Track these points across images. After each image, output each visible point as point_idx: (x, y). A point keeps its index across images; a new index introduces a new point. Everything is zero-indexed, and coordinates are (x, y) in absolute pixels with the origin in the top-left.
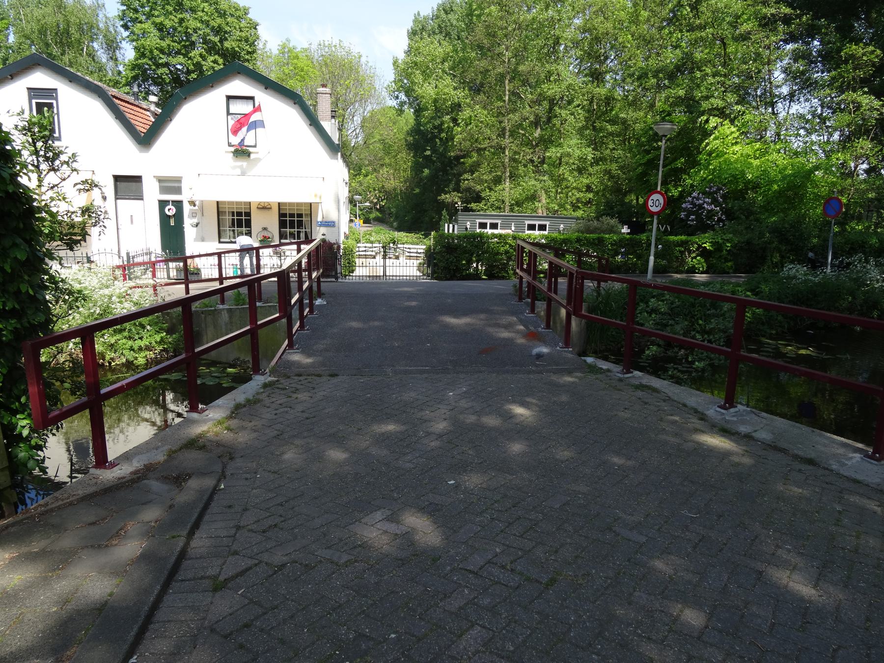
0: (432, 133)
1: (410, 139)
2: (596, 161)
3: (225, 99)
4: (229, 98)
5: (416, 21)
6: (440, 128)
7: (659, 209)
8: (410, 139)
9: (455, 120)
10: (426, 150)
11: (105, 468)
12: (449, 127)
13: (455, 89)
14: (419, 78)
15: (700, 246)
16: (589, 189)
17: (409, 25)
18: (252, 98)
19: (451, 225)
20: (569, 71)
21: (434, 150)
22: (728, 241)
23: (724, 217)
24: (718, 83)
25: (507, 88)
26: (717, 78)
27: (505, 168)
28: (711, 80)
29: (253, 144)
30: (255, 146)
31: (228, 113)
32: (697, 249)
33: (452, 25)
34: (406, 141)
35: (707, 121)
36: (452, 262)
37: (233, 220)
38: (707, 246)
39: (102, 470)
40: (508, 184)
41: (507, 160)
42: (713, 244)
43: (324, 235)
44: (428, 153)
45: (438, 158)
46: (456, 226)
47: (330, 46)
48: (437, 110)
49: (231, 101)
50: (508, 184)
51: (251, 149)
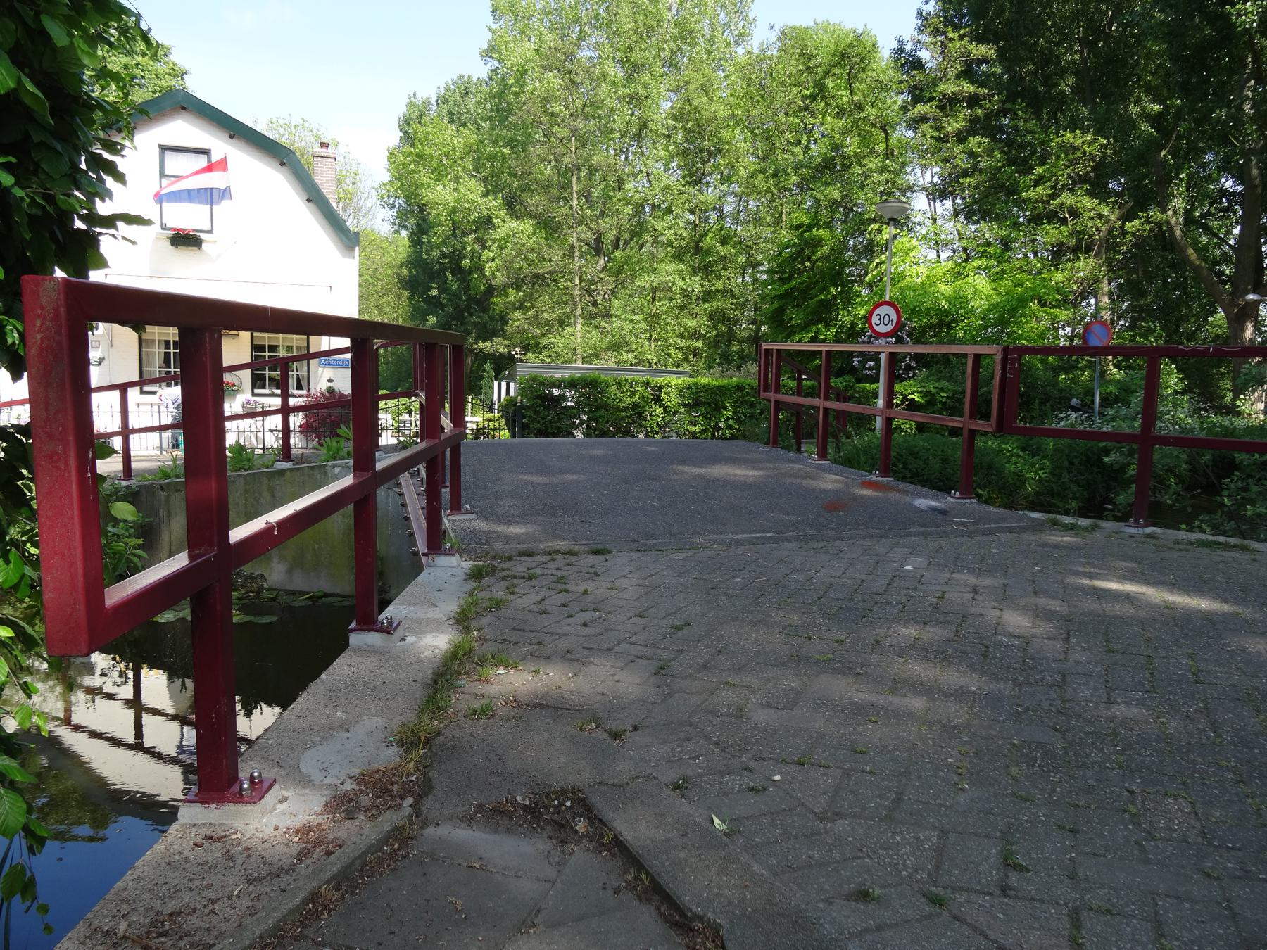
0: (440, 264)
1: (405, 272)
2: (707, 296)
3: (157, 150)
4: (164, 149)
5: (410, 105)
6: (455, 256)
7: (890, 328)
8: (405, 272)
9: (482, 242)
10: (430, 289)
11: (239, 798)
12: (473, 252)
13: (485, 195)
14: (424, 176)
15: (905, 398)
16: (695, 335)
17: (402, 110)
18: (206, 152)
19: (504, 384)
20: (655, 173)
21: (443, 289)
22: (942, 390)
23: (913, 364)
24: (887, 182)
25: (575, 188)
26: (885, 176)
27: (575, 304)
28: (876, 177)
29: (207, 227)
30: (210, 232)
31: (162, 175)
32: (903, 401)
33: (468, 112)
34: (398, 274)
35: (880, 231)
36: (551, 422)
37: (167, 355)
38: (916, 397)
39: (230, 808)
40: (579, 326)
41: (577, 292)
42: (925, 394)
43: (330, 381)
44: (434, 292)
45: (449, 300)
46: (512, 385)
47: (286, 126)
48: (455, 226)
49: (168, 155)
50: (579, 326)
51: (203, 236)
